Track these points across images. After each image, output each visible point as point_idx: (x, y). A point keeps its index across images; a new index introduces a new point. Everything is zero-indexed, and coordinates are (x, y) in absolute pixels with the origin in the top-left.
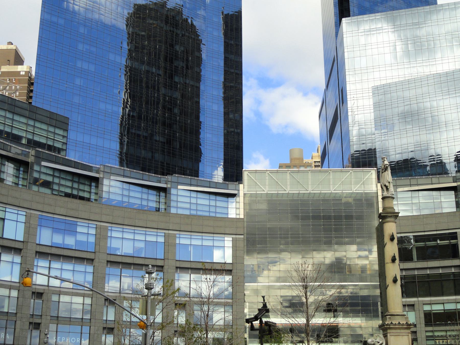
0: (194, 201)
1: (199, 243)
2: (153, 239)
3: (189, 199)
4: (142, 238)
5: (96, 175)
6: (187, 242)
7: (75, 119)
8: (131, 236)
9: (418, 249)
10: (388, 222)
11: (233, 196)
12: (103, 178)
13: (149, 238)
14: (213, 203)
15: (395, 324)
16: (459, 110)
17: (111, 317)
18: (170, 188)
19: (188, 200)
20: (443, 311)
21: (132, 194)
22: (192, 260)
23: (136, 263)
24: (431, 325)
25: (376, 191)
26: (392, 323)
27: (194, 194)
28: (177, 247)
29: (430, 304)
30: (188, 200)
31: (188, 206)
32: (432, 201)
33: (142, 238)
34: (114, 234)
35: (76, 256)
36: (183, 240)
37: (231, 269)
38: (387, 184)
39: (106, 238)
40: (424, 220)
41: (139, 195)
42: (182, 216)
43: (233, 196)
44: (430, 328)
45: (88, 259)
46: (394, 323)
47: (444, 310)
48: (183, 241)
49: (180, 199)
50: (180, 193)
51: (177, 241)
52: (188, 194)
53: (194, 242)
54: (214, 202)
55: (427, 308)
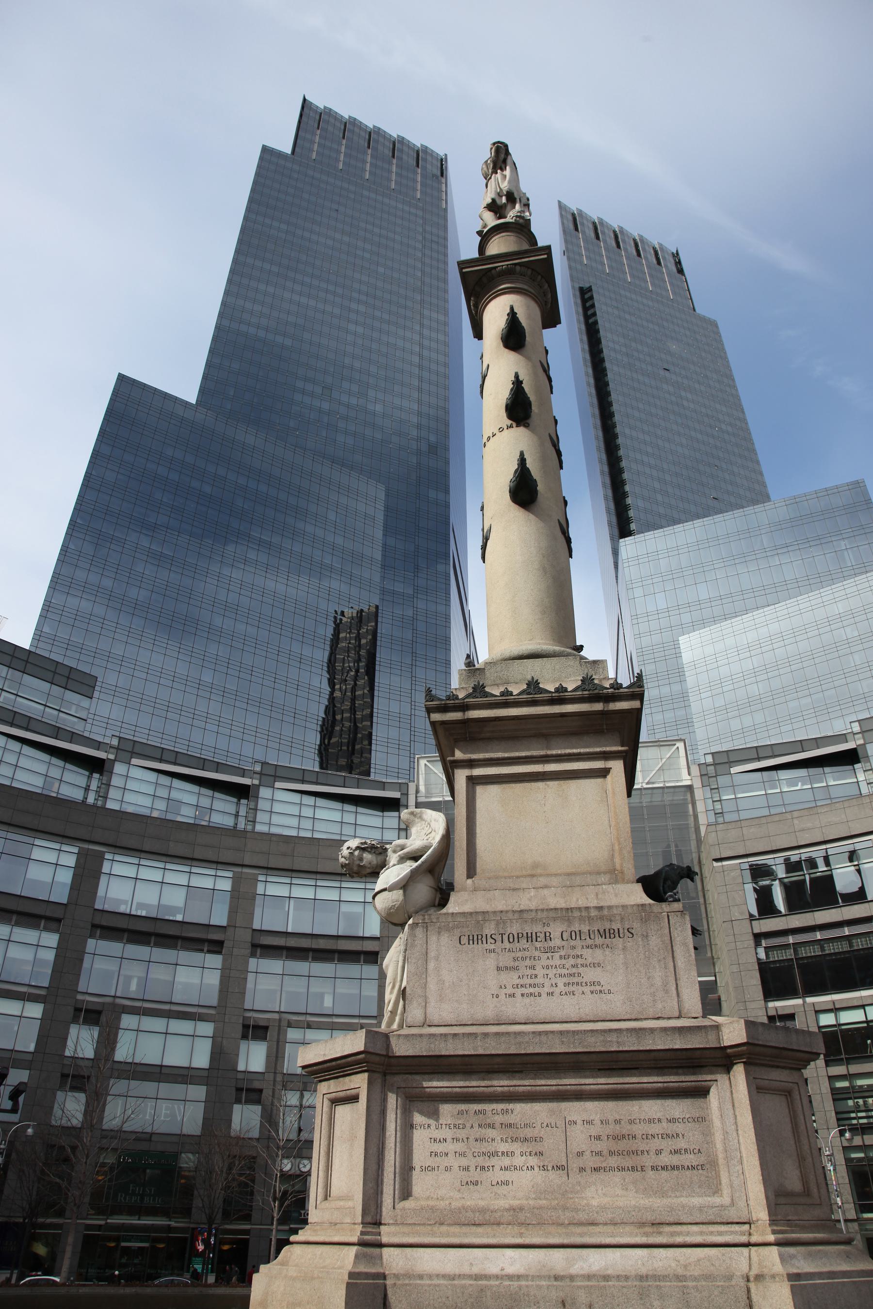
0: (307, 812)
1: (308, 893)
2: (208, 883)
3: (297, 808)
6: (283, 891)
7: (108, 678)
8: (157, 875)
12: (115, 760)
13: (196, 881)
14: (349, 818)
16: (870, 704)
17: (87, 1050)
18: (258, 787)
20: (865, 1025)
22: (290, 930)
23: (161, 932)
24: (838, 1062)
27: (310, 800)
28: (259, 900)
29: (835, 1010)
32: (810, 786)
33: (182, 879)
34: (118, 869)
35: (20, 909)
36: (274, 887)
37: (377, 949)
39: (97, 874)
40: (796, 822)
42: (274, 839)
44: (840, 1070)
45: (48, 919)
47: (867, 1022)
49: (277, 808)
51: (260, 889)
52: (296, 798)
53: (297, 892)
54: (162, 657)
55: (827, 1020)
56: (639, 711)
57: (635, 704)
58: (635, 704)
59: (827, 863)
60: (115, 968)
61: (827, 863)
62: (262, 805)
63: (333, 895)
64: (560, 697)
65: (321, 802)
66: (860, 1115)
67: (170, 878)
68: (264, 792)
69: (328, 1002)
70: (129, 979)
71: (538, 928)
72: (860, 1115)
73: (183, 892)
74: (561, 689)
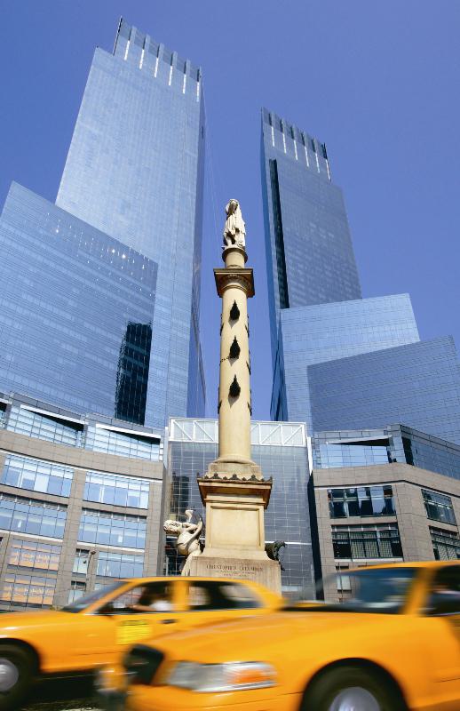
2: (60, 474)
4: (48, 472)
5: (6, 402)
9: (357, 502)
10: (229, 287)
11: (156, 441)
13: (54, 473)
15: (225, 481)
19: (106, 440)
21: (44, 426)
25: (304, 445)
26: (216, 476)
30: (106, 440)
31: (106, 446)
33: (48, 472)
38: (233, 232)
41: (53, 430)
43: (156, 441)
46: (221, 476)
48: (94, 480)
50: (98, 431)
56: (270, 490)
57: (268, 487)
58: (268, 487)
59: (368, 493)
60: (10, 516)
61: (368, 493)
62: (12, 416)
63: (124, 486)
64: (244, 482)
65: (45, 420)
66: (118, 557)
67: (41, 470)
68: (14, 410)
69: (120, 540)
70: (18, 521)
71: (340, 571)
72: (118, 557)
73: (47, 479)
74: (244, 479)
